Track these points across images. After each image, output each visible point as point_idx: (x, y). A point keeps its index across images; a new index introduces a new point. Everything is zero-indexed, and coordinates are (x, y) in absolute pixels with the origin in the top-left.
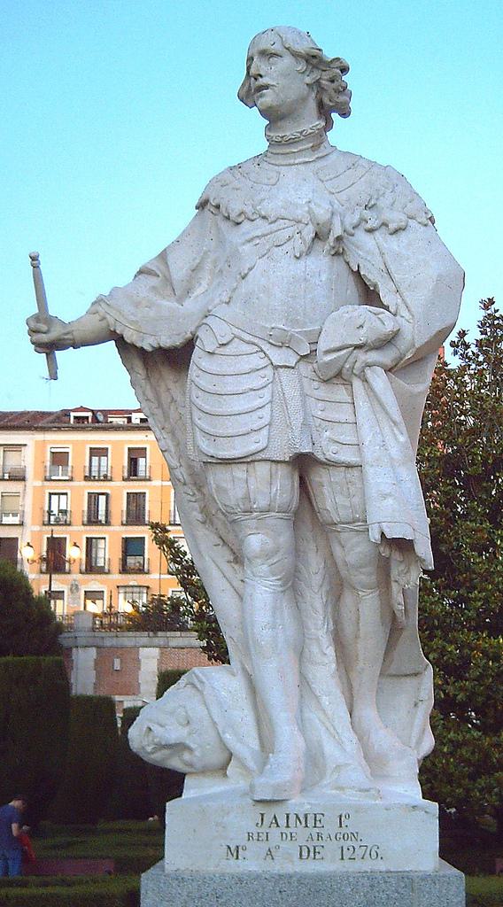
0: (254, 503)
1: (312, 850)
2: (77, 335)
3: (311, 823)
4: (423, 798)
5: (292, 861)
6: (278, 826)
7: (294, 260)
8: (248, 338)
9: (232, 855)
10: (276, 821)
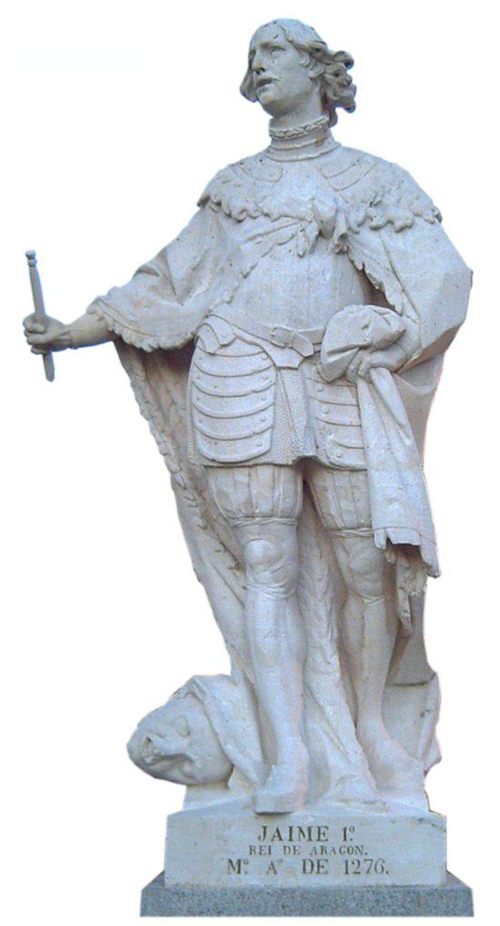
0: (257, 508)
3: (315, 836)
6: (281, 839)
9: (234, 868)
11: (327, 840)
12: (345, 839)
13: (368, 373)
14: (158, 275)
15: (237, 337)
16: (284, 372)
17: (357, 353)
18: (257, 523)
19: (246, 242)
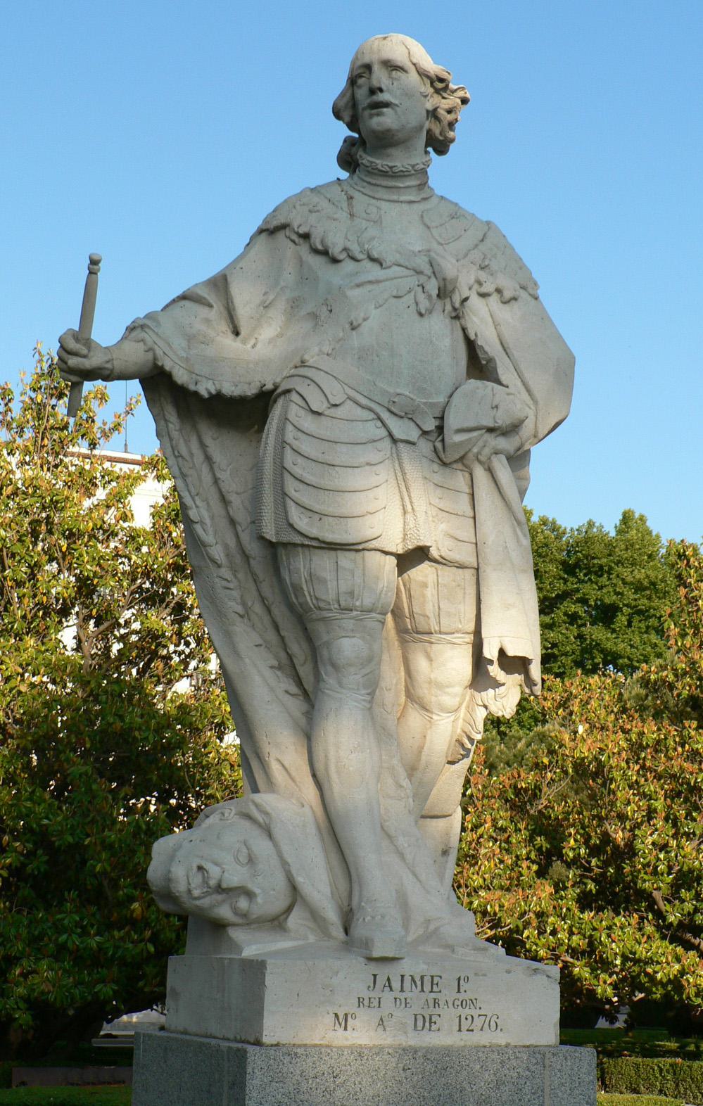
0: (357, 600)
1: (427, 1020)
2: (118, 366)
3: (427, 987)
4: (507, 954)
5: (405, 1033)
6: (391, 990)
7: (417, 317)
8: (364, 401)
9: (340, 1025)
10: (389, 983)
11: (440, 992)
12: (459, 991)
13: (490, 458)
14: (211, 306)
15: (349, 398)
16: (401, 445)
17: (482, 435)
18: (353, 618)
19: (352, 288)
